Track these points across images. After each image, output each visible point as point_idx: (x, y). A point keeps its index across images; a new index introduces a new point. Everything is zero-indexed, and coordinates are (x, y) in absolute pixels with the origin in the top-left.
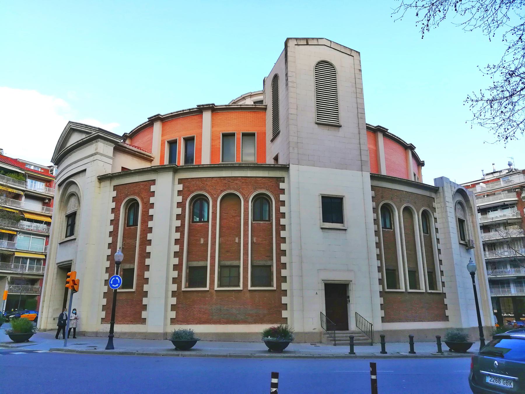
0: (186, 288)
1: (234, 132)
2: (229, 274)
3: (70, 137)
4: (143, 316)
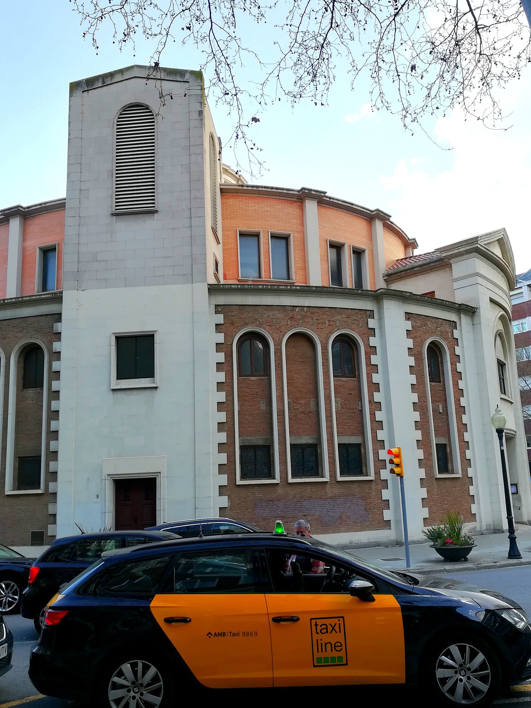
0: (14, 490)
2: (307, 459)
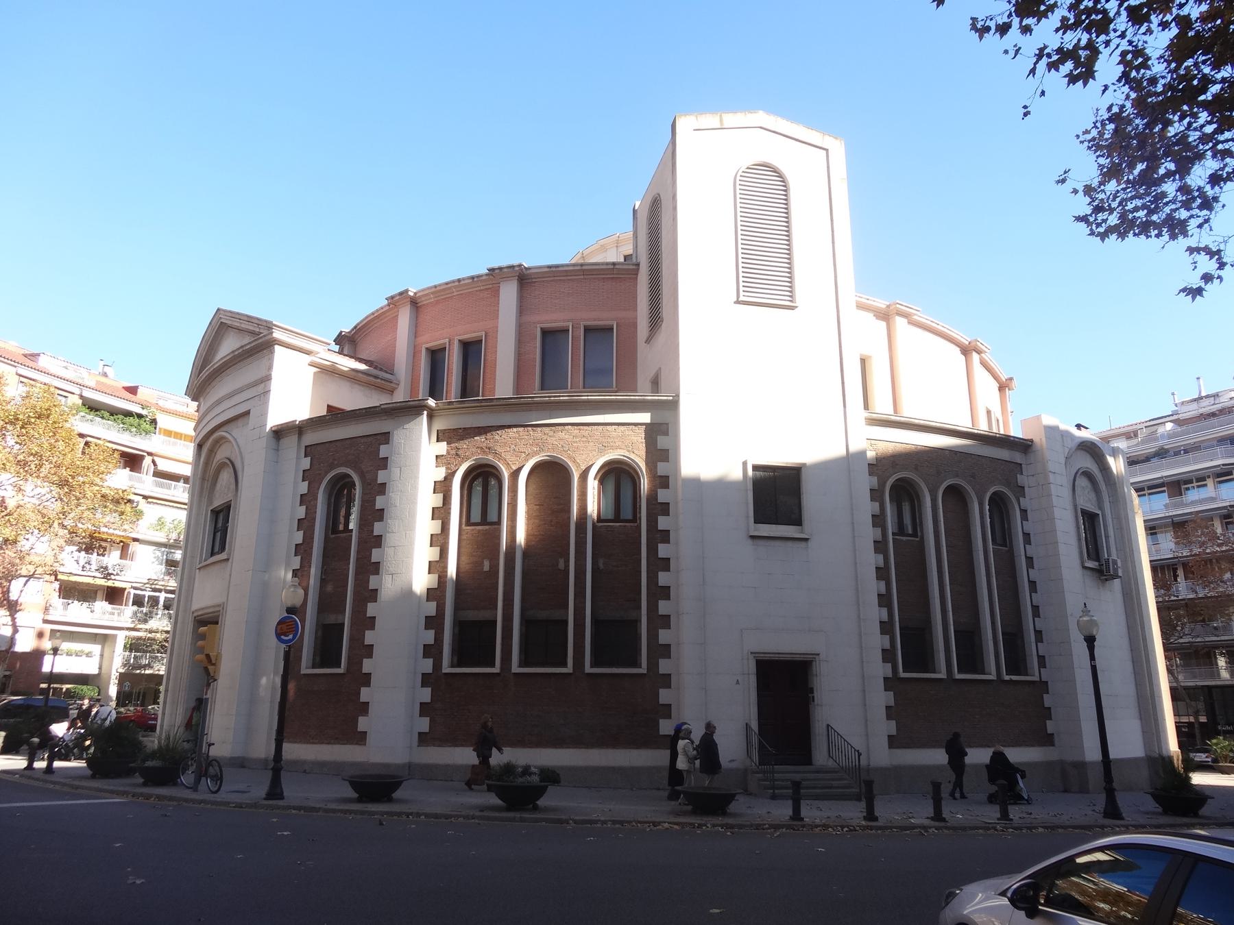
1: (565, 324)
3: (219, 344)
4: (361, 728)
